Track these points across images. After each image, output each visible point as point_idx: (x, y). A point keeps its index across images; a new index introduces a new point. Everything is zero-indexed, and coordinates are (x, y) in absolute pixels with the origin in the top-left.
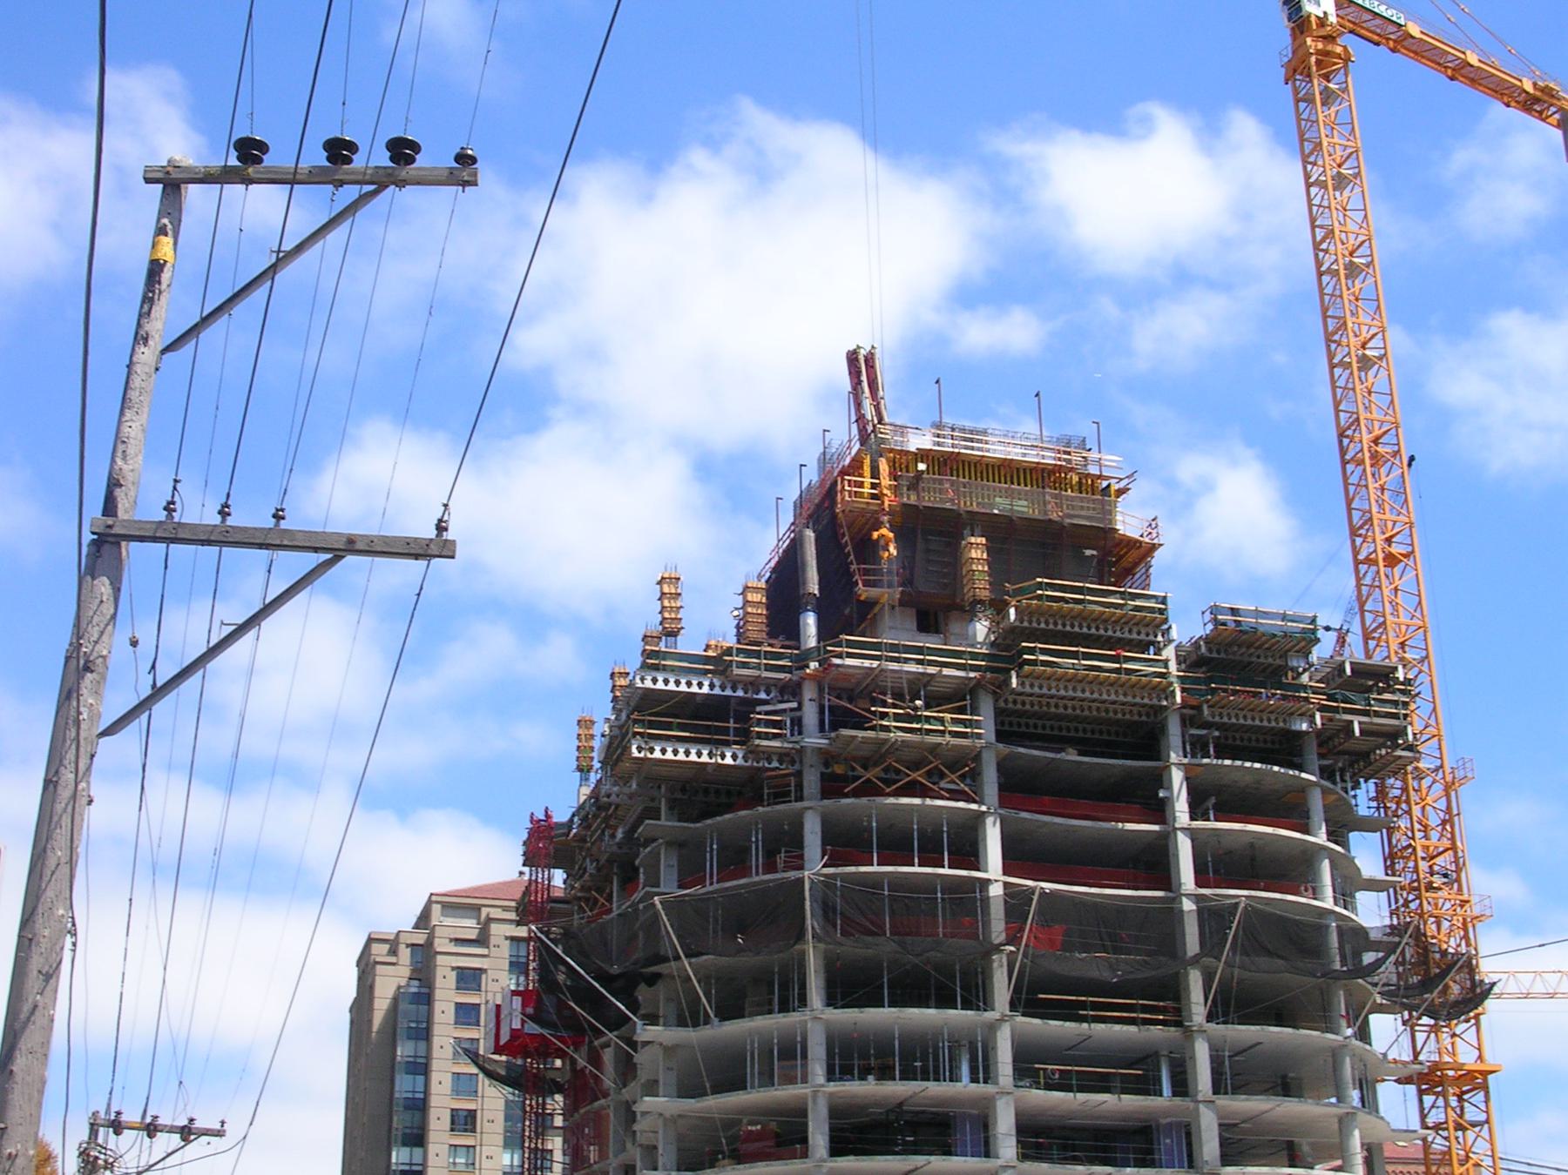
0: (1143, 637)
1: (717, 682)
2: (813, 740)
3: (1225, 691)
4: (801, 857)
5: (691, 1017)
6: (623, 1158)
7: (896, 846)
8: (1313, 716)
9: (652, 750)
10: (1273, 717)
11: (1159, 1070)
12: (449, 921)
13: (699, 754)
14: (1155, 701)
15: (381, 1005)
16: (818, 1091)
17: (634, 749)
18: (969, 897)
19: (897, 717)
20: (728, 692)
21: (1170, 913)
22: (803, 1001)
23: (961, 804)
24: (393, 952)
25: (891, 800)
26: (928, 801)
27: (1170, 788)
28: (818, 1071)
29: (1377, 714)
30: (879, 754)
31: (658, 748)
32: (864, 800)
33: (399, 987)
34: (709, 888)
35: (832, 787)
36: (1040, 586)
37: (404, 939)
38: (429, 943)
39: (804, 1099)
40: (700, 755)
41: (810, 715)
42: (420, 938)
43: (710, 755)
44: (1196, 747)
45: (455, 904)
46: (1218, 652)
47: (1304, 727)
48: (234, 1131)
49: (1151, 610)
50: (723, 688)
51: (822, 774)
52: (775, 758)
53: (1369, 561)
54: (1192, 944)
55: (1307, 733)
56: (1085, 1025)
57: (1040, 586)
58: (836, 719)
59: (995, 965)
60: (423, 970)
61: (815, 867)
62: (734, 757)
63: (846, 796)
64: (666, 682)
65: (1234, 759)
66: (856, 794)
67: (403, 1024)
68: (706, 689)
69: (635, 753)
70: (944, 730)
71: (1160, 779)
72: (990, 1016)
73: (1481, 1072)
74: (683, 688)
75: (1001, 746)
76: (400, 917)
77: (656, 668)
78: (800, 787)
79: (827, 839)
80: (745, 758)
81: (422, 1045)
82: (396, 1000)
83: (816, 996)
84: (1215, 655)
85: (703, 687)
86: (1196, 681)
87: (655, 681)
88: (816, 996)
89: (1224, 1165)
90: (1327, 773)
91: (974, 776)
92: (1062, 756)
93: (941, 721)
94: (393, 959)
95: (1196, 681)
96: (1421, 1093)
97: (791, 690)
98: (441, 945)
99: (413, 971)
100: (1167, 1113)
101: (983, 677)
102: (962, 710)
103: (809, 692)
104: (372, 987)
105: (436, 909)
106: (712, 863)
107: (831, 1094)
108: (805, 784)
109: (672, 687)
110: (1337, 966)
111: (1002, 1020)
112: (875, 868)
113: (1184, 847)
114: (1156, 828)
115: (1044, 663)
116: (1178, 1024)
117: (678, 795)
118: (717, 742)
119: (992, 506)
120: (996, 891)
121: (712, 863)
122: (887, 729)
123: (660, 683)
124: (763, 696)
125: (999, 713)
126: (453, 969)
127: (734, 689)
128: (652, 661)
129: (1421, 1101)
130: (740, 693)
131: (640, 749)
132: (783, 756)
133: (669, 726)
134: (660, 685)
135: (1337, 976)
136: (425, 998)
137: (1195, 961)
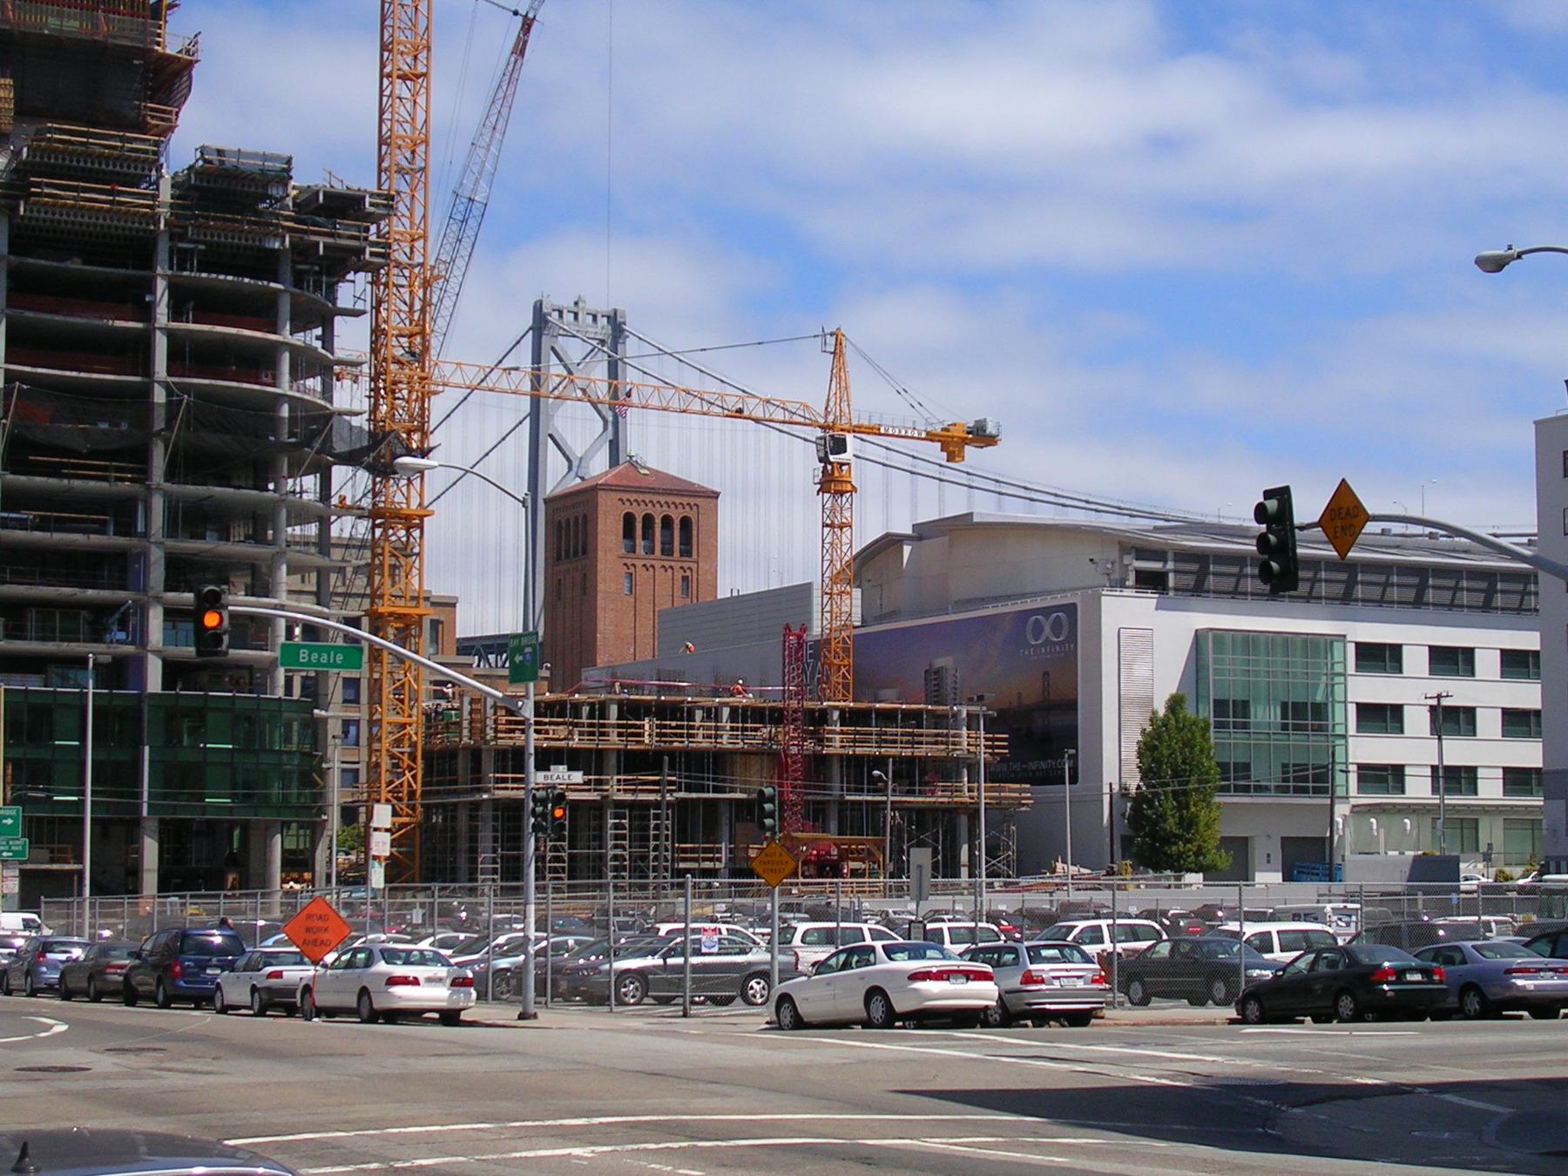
0: (139, 171)
3: (207, 218)
21: (145, 392)
27: (153, 293)
36: (50, 130)
44: (181, 259)
47: (277, 245)
49: (146, 151)
53: (389, 76)
54: (159, 424)
56: (66, 481)
57: (50, 130)
65: (210, 272)
86: (183, 207)
89: (166, 590)
92: (62, 265)
95: (183, 207)
110: (285, 438)
114: (140, 325)
119: (46, 25)
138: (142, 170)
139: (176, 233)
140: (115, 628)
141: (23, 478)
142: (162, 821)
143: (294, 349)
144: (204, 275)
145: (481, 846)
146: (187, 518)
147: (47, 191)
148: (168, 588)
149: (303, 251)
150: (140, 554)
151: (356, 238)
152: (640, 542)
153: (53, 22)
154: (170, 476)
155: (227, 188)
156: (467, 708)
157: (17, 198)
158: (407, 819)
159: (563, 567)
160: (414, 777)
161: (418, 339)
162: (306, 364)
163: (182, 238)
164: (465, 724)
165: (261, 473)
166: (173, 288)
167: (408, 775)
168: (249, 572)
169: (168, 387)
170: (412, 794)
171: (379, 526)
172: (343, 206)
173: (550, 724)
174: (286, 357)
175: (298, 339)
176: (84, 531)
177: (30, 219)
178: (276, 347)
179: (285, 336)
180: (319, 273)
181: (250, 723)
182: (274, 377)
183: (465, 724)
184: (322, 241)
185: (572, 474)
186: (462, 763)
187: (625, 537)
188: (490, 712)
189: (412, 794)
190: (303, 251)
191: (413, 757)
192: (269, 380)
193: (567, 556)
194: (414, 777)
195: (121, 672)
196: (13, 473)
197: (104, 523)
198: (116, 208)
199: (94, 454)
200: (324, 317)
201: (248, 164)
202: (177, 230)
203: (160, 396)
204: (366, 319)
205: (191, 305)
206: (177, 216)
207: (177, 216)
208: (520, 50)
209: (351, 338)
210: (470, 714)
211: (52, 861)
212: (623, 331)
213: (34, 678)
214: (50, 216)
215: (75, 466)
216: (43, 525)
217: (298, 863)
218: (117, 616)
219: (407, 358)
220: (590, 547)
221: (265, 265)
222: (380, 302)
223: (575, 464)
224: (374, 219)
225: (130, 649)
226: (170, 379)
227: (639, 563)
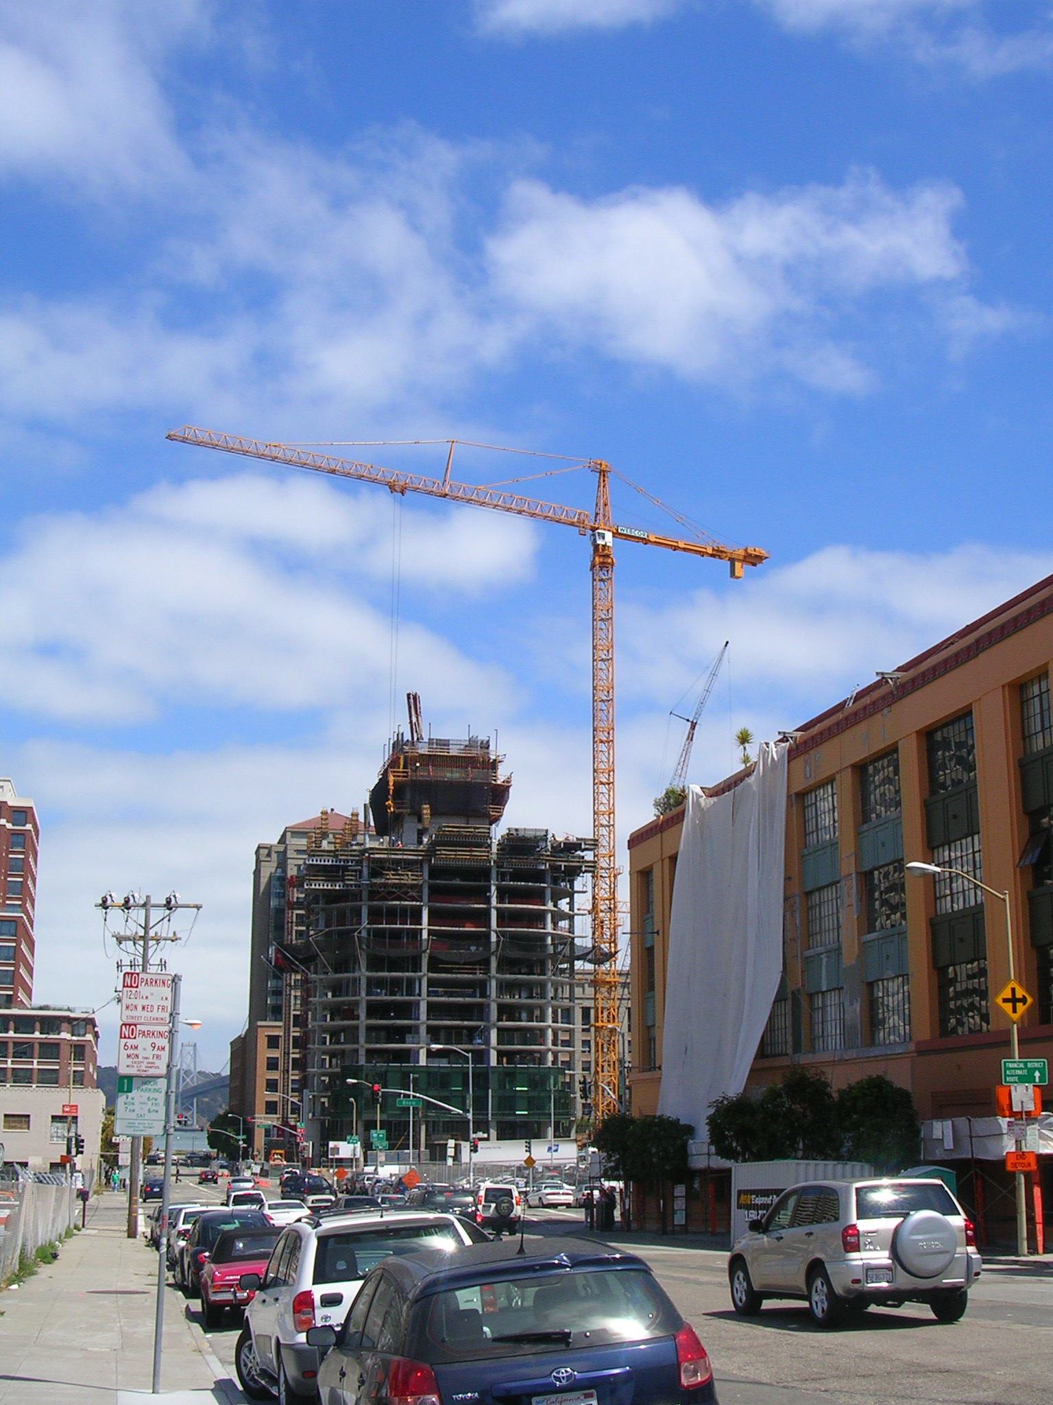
7: (392, 915)
15: (264, 881)
18: (417, 933)
24: (269, 855)
35: (371, 898)
38: (285, 852)
42: (281, 849)
44: (502, 876)
45: (296, 832)
48: (184, 939)
58: (374, 873)
61: (365, 923)
66: (379, 900)
67: (273, 891)
70: (408, 878)
85: (329, 862)
88: (363, 970)
91: (420, 891)
97: (359, 863)
98: (290, 854)
105: (289, 834)
113: (494, 913)
138: (482, 841)
139: (499, 864)
149: (555, 869)
153: (449, 775)
155: (521, 846)
162: (558, 916)
166: (498, 889)
172: (571, 847)
174: (549, 916)
181: (538, 1081)
195: (480, 1056)
201: (529, 834)
203: (494, 938)
208: (690, 738)
209: (583, 902)
213: (445, 1060)
221: (539, 876)
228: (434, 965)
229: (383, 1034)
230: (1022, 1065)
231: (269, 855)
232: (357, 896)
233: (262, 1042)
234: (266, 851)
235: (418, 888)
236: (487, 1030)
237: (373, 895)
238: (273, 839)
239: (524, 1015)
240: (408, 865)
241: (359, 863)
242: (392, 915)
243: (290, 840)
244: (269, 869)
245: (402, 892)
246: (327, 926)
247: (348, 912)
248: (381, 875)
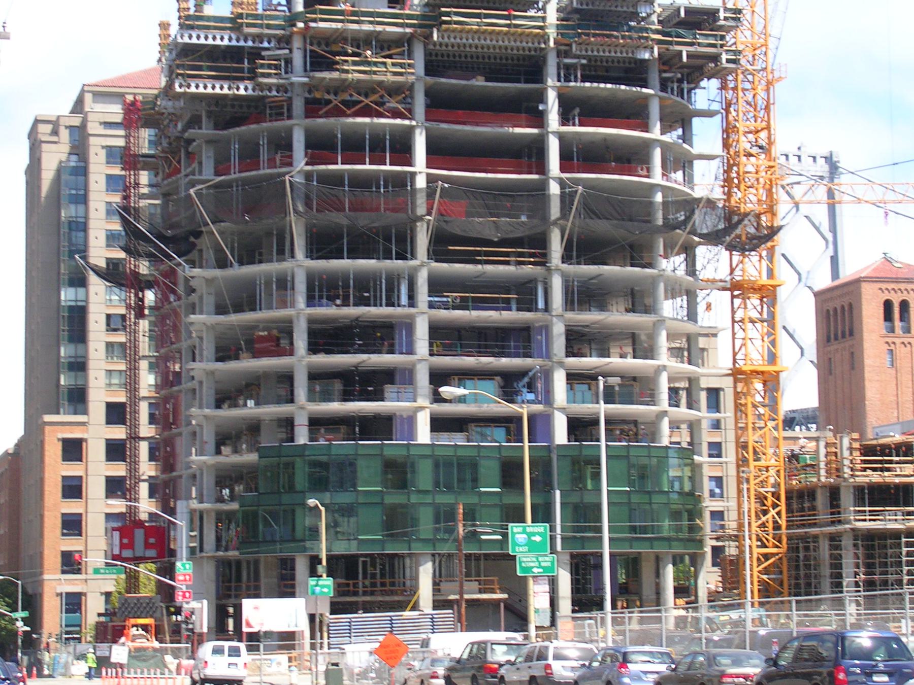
1: (234, 36)
2: (298, 79)
3: (588, 35)
4: (291, 157)
5: (222, 263)
6: (189, 342)
7: (354, 147)
8: (652, 48)
9: (189, 86)
10: (624, 50)
11: (536, 295)
12: (99, 107)
13: (222, 88)
14: (536, 45)
16: (301, 312)
17: (177, 85)
18: (403, 182)
19: (355, 63)
20: (242, 43)
21: (542, 187)
22: (293, 256)
23: (398, 121)
24: (55, 132)
25: (350, 120)
26: (376, 120)
27: (546, 103)
28: (301, 300)
29: (699, 44)
30: (339, 87)
31: (193, 85)
32: (332, 120)
33: (61, 162)
34: (233, 176)
37: (62, 122)
38: (83, 127)
39: (291, 316)
40: (222, 89)
41: (298, 59)
42: (76, 121)
43: (229, 89)
44: (566, 73)
46: (587, 5)
50: (238, 40)
51: (306, 99)
52: (274, 88)
54: (555, 211)
55: (649, 60)
56: (480, 267)
59: (418, 229)
60: (80, 148)
61: (300, 162)
62: (246, 89)
63: (320, 117)
64: (198, 37)
66: (327, 115)
67: (65, 192)
68: (226, 42)
69: (178, 89)
70: (387, 71)
71: (541, 97)
72: (412, 263)
73: (771, 286)
74: (210, 42)
75: (428, 78)
76: (60, 106)
77: (192, 27)
78: (290, 109)
79: (308, 146)
80: (254, 90)
81: (81, 208)
82: (59, 171)
83: (300, 253)
84: (584, 7)
85: (224, 40)
87: (190, 37)
88: (300, 253)
89: (567, 356)
90: (664, 85)
93: (384, 64)
94: (55, 139)
96: (733, 297)
97: (285, 41)
98: (93, 128)
99: (72, 148)
100: (538, 321)
101: (415, 32)
102: (401, 54)
103: (297, 43)
104: (39, 160)
105: (88, 97)
106: (235, 161)
107: (309, 314)
108: (294, 106)
109: (202, 41)
111: (422, 265)
112: (339, 167)
114: (535, 131)
115: (456, 23)
116: (543, 264)
117: (214, 108)
118: (233, 78)
120: (421, 182)
121: (235, 161)
122: (347, 72)
123: (195, 39)
124: (266, 45)
125: (428, 54)
126: (103, 147)
127: (246, 41)
128: (188, 22)
129: (732, 303)
130: (250, 43)
131: (181, 86)
132: (279, 88)
133: (199, 68)
134: (194, 41)
135: (659, 230)
136: (82, 171)
137: (555, 223)
140: (525, 390)
141: (445, 265)
142: (572, 556)
143: (665, 147)
144: (588, 84)
145: (844, 572)
146: (583, 295)
147: (456, 18)
148: (570, 353)
149: (668, 61)
150: (541, 327)
151: (714, 46)
152: (898, 324)
154: (567, 258)
156: (823, 451)
157: (432, 27)
158: (775, 550)
159: (832, 348)
160: (779, 513)
161: (763, 135)
163: (567, 54)
164: (822, 465)
165: (638, 254)
167: (773, 512)
168: (630, 341)
169: (562, 183)
170: (777, 527)
171: (737, 296)
173: (897, 463)
175: (667, 138)
176: (496, 309)
177: (441, 45)
178: (647, 145)
179: (655, 133)
180: (680, 81)
182: (648, 170)
183: (822, 465)
184: (685, 50)
185: (802, 284)
186: (821, 500)
187: (885, 320)
188: (846, 453)
189: (777, 527)
190: (668, 61)
191: (776, 495)
192: (645, 173)
193: (836, 339)
194: (779, 513)
196: (436, 261)
197: (508, 301)
198: (513, 30)
199: (503, 243)
200: (680, 119)
202: (563, 48)
203: (554, 189)
204: (718, 118)
205: (577, 111)
206: (562, 34)
207: (562, 34)
209: (706, 136)
210: (826, 456)
211: (480, 592)
212: (837, 168)
214: (458, 40)
215: (487, 254)
216: (463, 305)
217: (684, 590)
218: (526, 380)
219: (755, 150)
220: (855, 331)
221: (635, 73)
222: (729, 105)
223: (804, 276)
224: (728, 29)
225: (539, 407)
226: (565, 175)
227: (898, 341)
228: (441, 247)
229: (338, 386)
230: (534, 559)
231: (55, 132)
232: (281, 110)
233: (53, 451)
234: (48, 128)
235: (402, 92)
236: (547, 376)
237: (313, 108)
238: (62, 107)
239: (125, 541)
240: (386, 45)
241: (285, 41)
242: (354, 147)
243: (89, 103)
244: (55, 156)
245: (370, 99)
246: (217, 174)
247: (263, 142)
248: (330, 66)
